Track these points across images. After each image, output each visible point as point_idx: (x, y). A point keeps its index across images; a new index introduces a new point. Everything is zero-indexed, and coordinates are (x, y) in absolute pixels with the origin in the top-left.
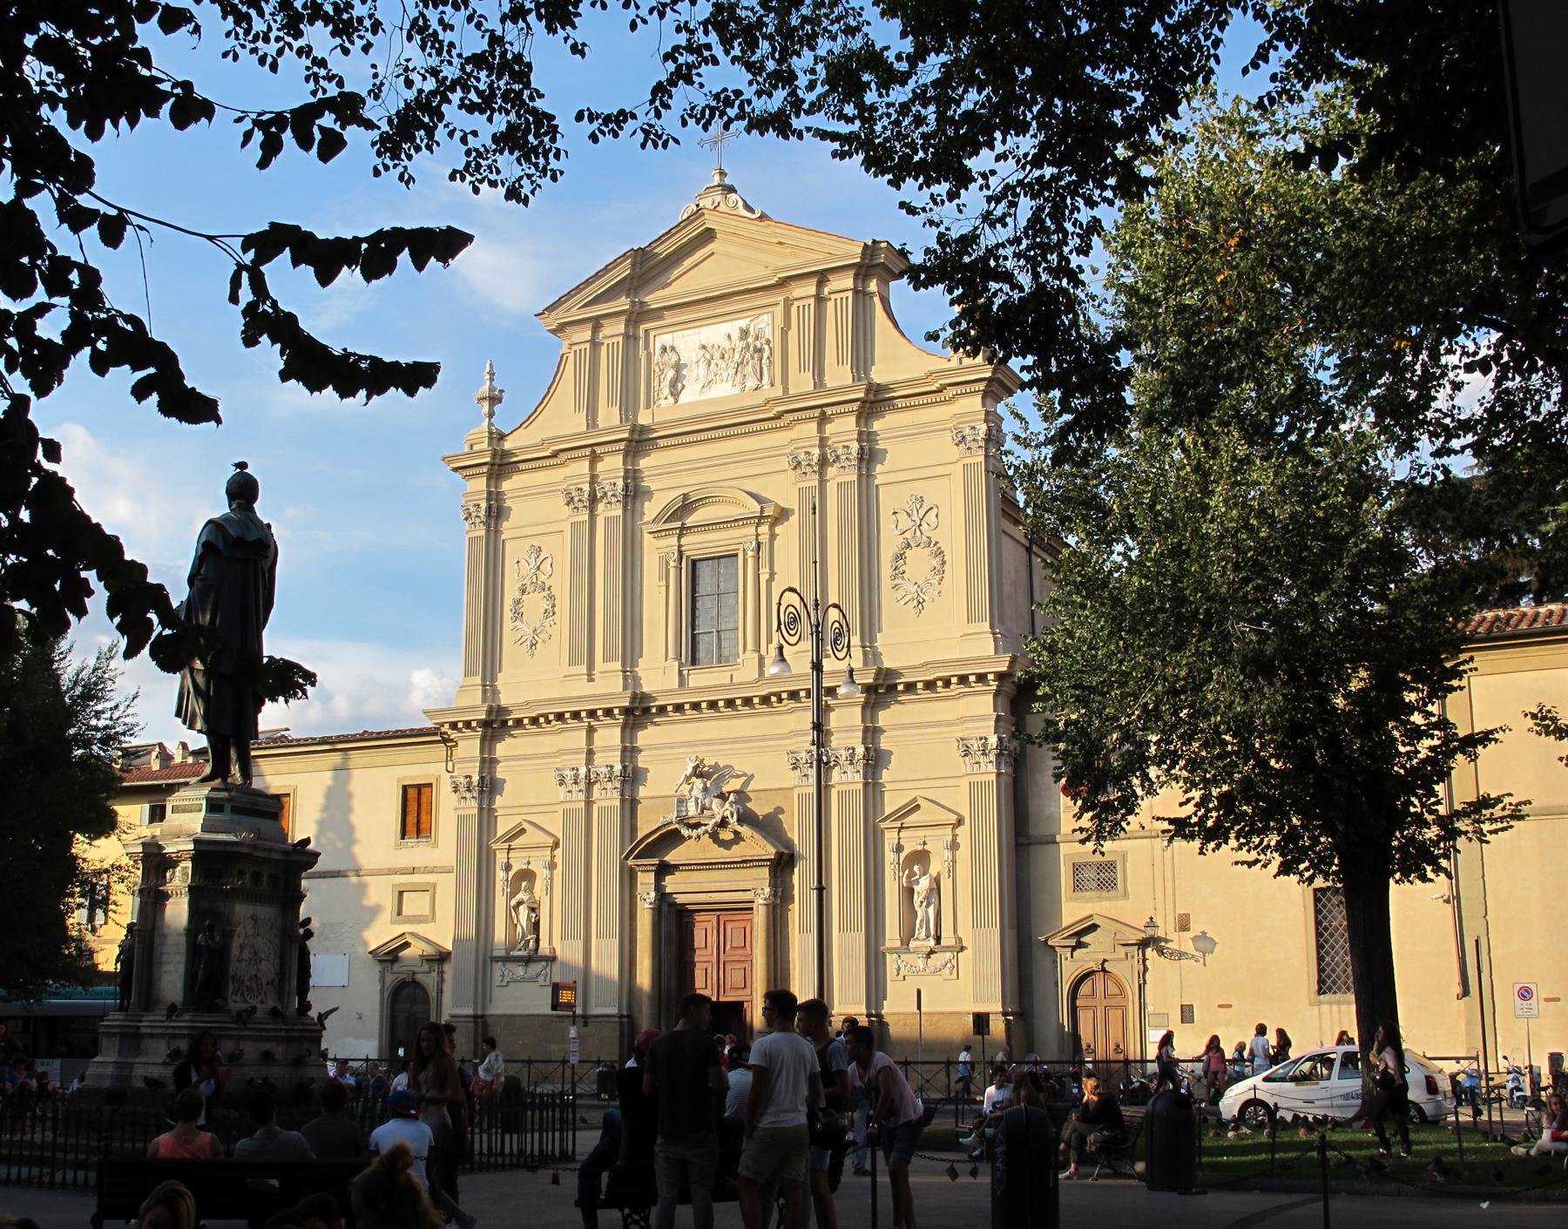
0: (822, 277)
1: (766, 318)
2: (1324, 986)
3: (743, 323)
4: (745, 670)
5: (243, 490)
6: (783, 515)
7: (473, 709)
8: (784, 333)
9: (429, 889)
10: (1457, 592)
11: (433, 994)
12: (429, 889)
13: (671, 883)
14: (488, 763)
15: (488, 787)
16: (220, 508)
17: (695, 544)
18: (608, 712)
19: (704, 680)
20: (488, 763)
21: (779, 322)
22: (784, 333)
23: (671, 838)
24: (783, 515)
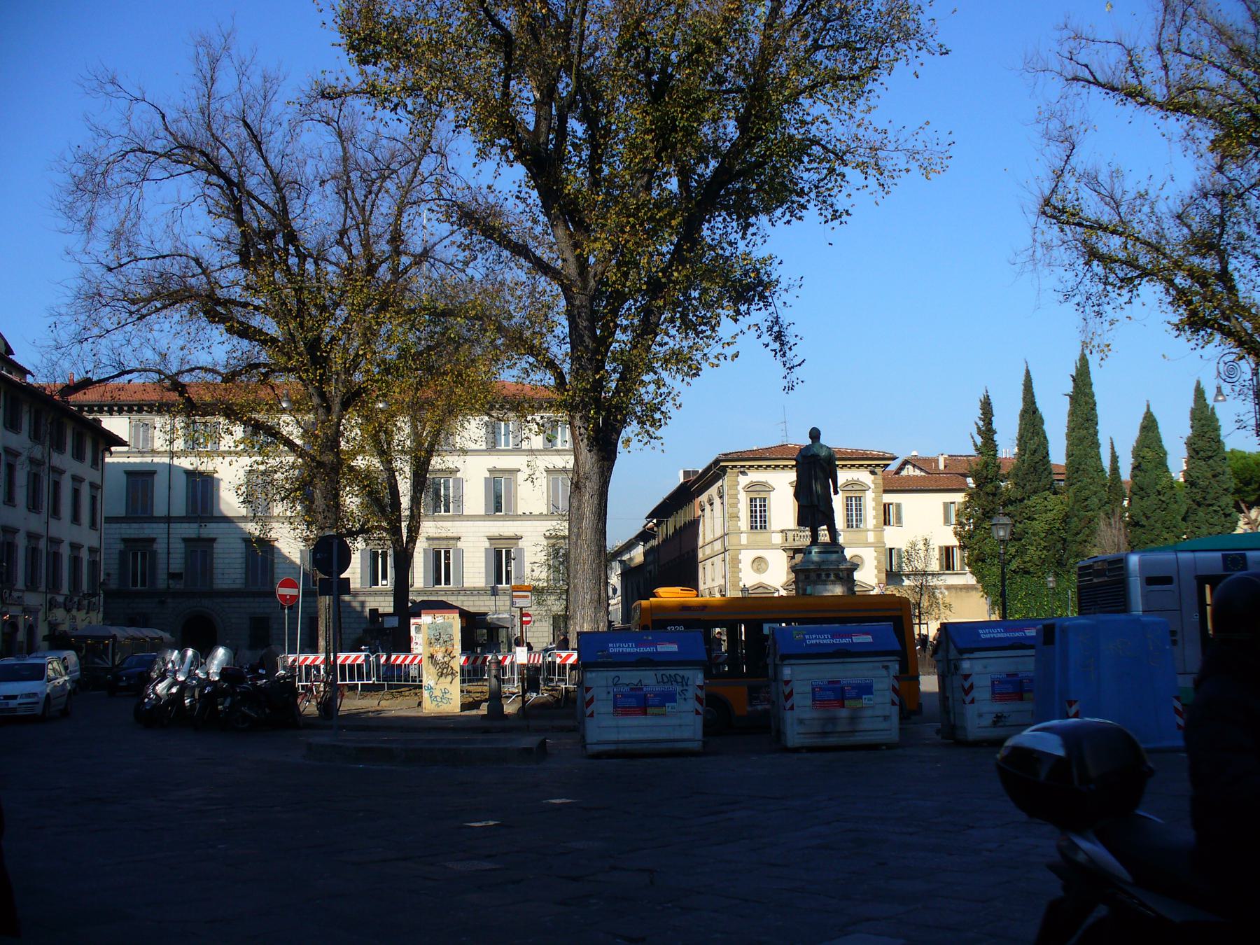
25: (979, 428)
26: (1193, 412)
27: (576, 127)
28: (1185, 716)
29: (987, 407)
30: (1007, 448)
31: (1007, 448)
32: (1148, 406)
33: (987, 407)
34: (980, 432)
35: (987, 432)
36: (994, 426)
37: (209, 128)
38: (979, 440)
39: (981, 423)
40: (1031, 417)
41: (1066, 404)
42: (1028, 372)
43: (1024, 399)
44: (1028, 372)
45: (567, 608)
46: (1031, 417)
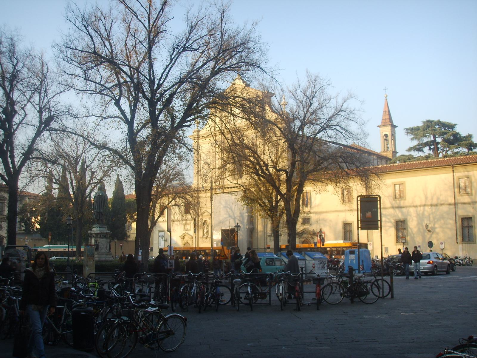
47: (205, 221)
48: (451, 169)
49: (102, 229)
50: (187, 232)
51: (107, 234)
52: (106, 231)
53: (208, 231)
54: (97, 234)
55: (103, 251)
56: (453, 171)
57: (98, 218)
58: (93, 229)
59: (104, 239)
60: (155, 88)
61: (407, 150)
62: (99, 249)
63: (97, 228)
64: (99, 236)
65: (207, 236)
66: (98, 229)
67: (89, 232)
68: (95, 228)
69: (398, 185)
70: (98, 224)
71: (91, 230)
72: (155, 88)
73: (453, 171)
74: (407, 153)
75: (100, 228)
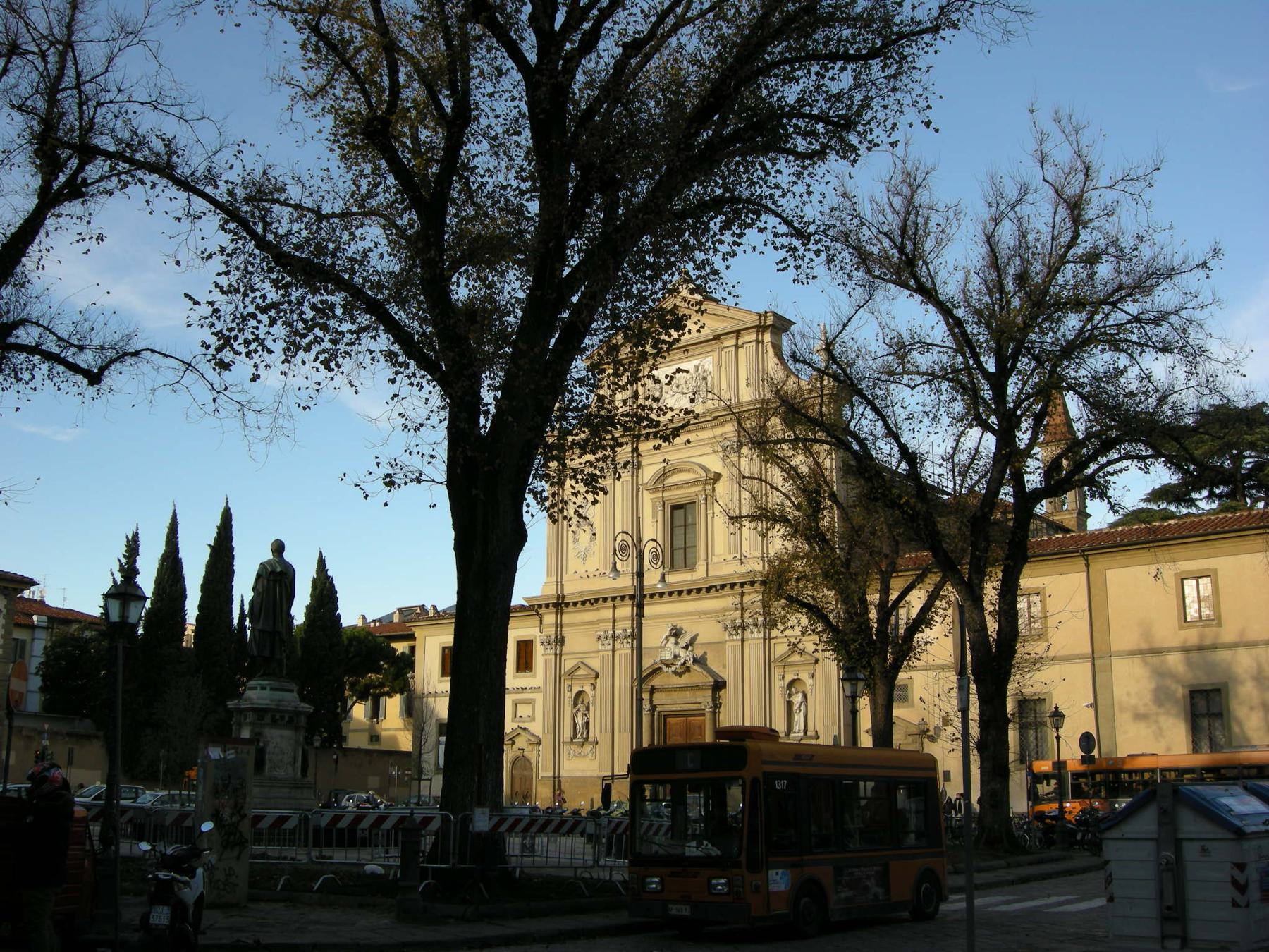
0: (738, 333)
1: (710, 359)
2: (443, 674)
3: (696, 362)
4: (700, 572)
5: (279, 548)
6: (718, 477)
7: (626, 588)
8: (719, 366)
9: (531, 702)
10: (19, 634)
11: (534, 764)
12: (531, 702)
13: (659, 698)
14: (559, 626)
15: (560, 641)
16: (268, 555)
17: (675, 496)
18: (623, 598)
19: (675, 578)
20: (559, 626)
21: (716, 362)
22: (719, 366)
23: (656, 671)
24: (718, 477)
25: (121, 565)
26: (314, 581)
27: (1019, 412)
28: (101, 734)
29: (133, 548)
30: (147, 581)
31: (147, 581)
32: (322, 563)
33: (133, 548)
34: (122, 569)
35: (129, 571)
36: (138, 565)
37: (111, 102)
38: (119, 578)
39: (124, 561)
40: (171, 565)
41: (206, 555)
42: (227, 518)
43: (168, 543)
44: (227, 518)
45: (752, 583)
46: (171, 565)
47: (579, 694)
48: (1082, 562)
49: (278, 695)
50: (522, 725)
51: (298, 713)
52: (290, 699)
53: (588, 723)
54: (260, 712)
55: (281, 773)
56: (1088, 566)
57: (267, 653)
58: (249, 693)
59: (287, 733)
60: (557, 26)
61: (1147, 500)
62: (267, 766)
63: (263, 688)
64: (268, 719)
65: (586, 739)
66: (267, 693)
67: (231, 704)
68: (255, 688)
69: (1194, 582)
70: (265, 676)
71: (240, 696)
72: (557, 26)
73: (1088, 566)
74: (1143, 505)
75: (272, 689)
